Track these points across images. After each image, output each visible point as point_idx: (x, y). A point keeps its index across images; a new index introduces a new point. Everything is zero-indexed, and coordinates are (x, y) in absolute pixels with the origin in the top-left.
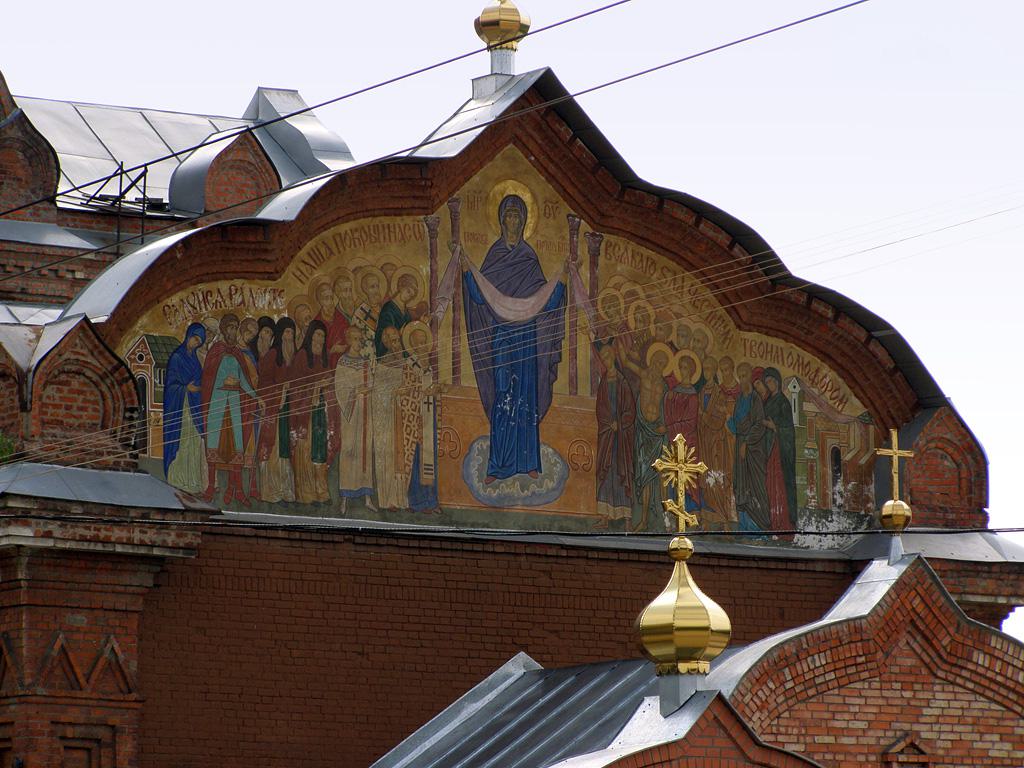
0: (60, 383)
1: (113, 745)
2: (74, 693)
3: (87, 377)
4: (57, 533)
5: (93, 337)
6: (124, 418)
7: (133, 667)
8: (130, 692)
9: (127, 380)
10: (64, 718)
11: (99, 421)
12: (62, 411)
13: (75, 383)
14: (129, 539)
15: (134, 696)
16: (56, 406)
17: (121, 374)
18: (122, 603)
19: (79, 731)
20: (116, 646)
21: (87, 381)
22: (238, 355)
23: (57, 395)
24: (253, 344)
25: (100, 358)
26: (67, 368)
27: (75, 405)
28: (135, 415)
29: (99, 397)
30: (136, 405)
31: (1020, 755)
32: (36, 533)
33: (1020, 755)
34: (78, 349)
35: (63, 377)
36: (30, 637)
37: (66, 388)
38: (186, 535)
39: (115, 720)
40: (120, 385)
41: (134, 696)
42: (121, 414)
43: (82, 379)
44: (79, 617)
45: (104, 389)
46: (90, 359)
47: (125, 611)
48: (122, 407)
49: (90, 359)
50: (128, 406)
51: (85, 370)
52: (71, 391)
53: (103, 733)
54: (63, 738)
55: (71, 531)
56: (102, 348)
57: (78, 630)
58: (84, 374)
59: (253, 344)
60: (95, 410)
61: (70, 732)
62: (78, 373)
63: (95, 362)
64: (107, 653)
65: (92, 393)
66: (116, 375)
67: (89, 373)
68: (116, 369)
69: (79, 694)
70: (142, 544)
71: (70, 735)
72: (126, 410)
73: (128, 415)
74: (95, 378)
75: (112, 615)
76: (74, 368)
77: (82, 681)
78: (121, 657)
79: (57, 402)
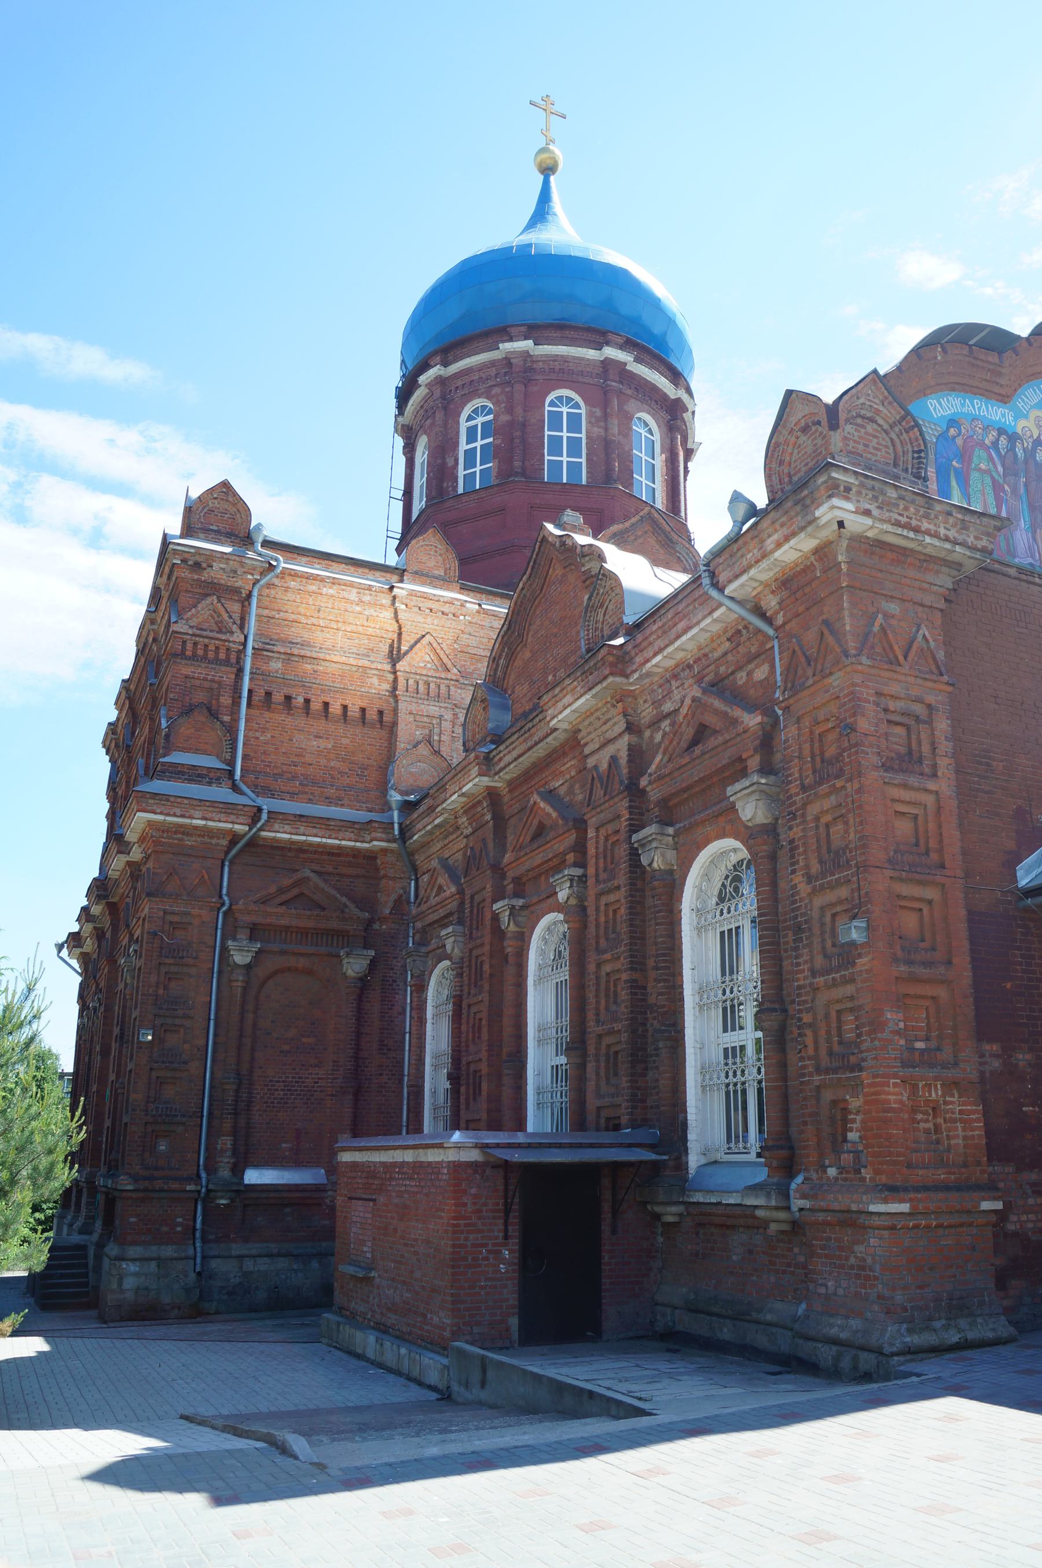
0: (858, 425)
1: (930, 722)
2: (894, 667)
3: (879, 425)
4: (876, 512)
5: (883, 389)
6: (913, 458)
7: (941, 655)
8: (941, 674)
9: (913, 428)
10: (886, 690)
11: (892, 462)
12: (861, 447)
13: (870, 427)
14: (936, 532)
15: (946, 678)
16: (855, 441)
17: (908, 422)
18: (928, 600)
19: (900, 705)
20: (927, 634)
21: (879, 429)
22: (987, 449)
23: (856, 434)
24: (995, 444)
25: (890, 408)
26: (863, 412)
27: (871, 444)
28: (922, 455)
29: (890, 444)
30: (922, 448)
31: (1039, 1201)
32: (857, 508)
33: (1039, 1201)
34: (871, 398)
35: (859, 421)
36: (851, 615)
37: (863, 431)
38: (982, 539)
39: (931, 699)
40: (907, 432)
41: (946, 678)
42: (910, 454)
43: (875, 426)
44: (893, 606)
45: (894, 436)
46: (881, 408)
47: (931, 607)
48: (910, 449)
49: (881, 408)
50: (916, 449)
51: (877, 418)
52: (866, 433)
53: (919, 709)
54: (886, 710)
55: (887, 514)
56: (891, 399)
57: (893, 616)
58: (876, 422)
59: (995, 444)
60: (887, 452)
61: (892, 705)
62: (872, 420)
63: (885, 411)
64: (920, 638)
65: (883, 439)
66: (904, 424)
67: (880, 421)
68: (903, 418)
69: (898, 669)
70: (947, 539)
71: (892, 708)
72: (914, 452)
73: (916, 455)
74: (886, 427)
75: (920, 609)
76: (869, 415)
77: (901, 658)
78: (932, 644)
79: (856, 438)
